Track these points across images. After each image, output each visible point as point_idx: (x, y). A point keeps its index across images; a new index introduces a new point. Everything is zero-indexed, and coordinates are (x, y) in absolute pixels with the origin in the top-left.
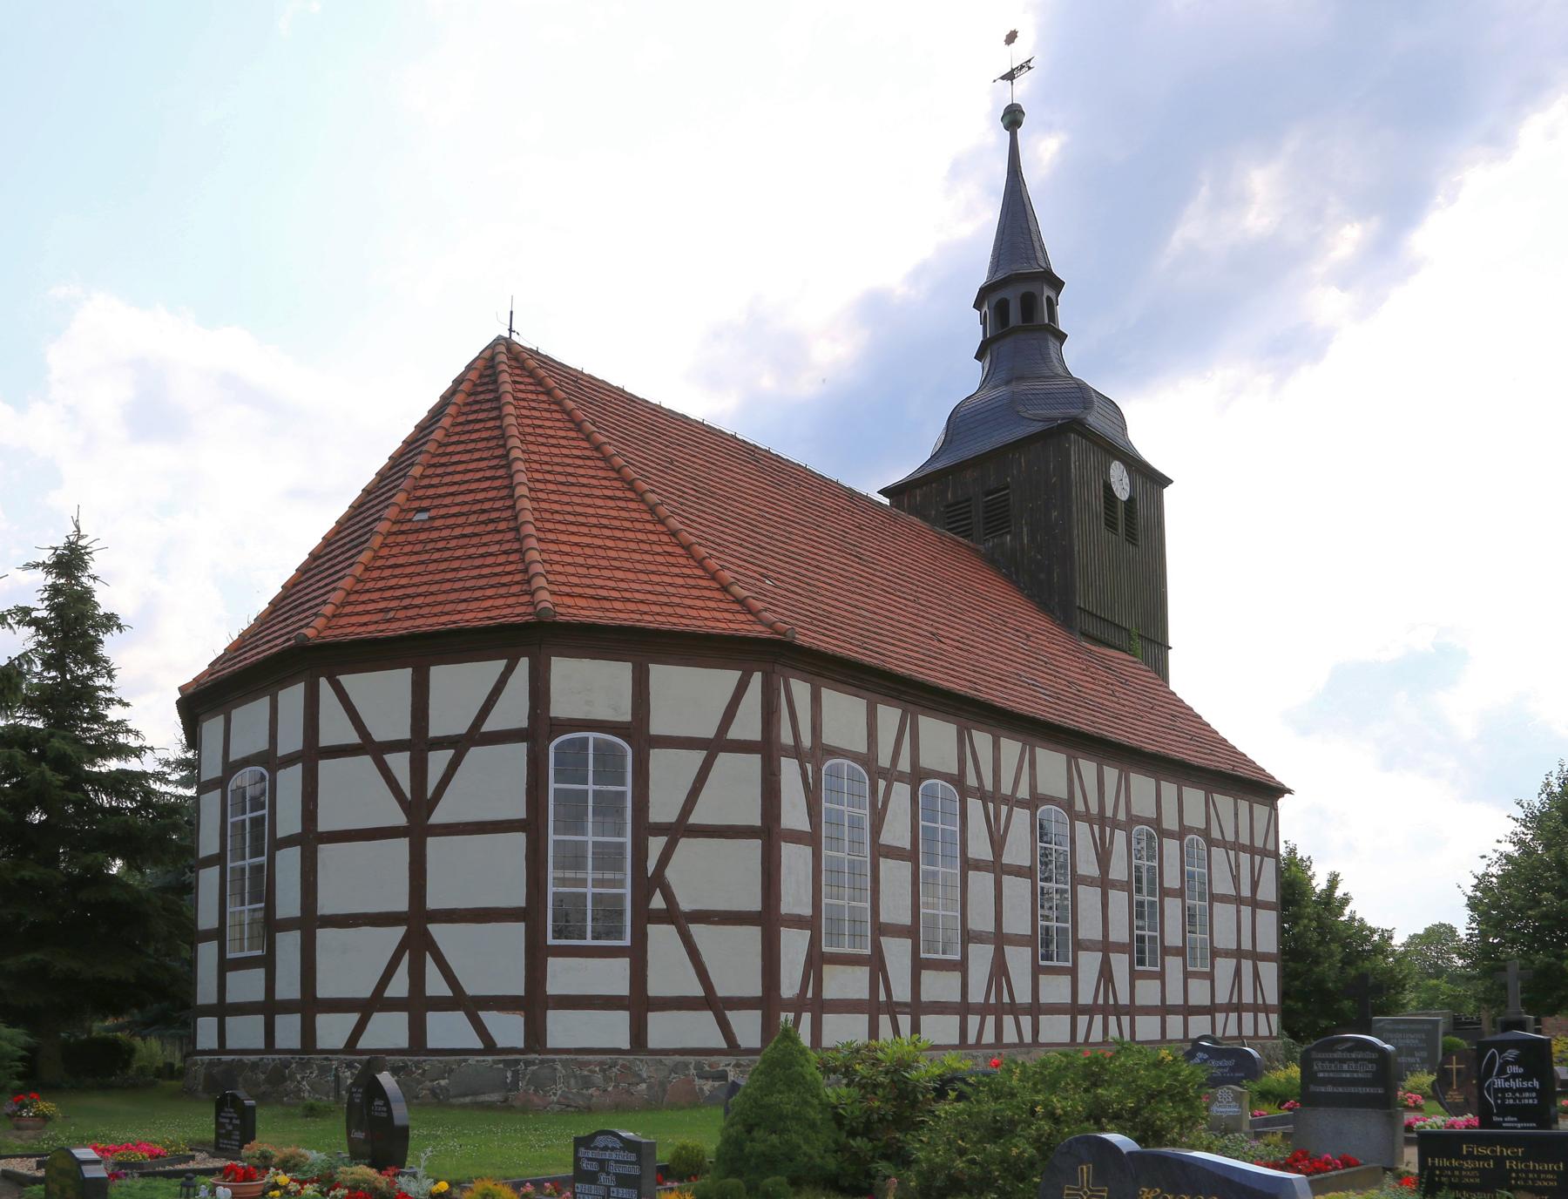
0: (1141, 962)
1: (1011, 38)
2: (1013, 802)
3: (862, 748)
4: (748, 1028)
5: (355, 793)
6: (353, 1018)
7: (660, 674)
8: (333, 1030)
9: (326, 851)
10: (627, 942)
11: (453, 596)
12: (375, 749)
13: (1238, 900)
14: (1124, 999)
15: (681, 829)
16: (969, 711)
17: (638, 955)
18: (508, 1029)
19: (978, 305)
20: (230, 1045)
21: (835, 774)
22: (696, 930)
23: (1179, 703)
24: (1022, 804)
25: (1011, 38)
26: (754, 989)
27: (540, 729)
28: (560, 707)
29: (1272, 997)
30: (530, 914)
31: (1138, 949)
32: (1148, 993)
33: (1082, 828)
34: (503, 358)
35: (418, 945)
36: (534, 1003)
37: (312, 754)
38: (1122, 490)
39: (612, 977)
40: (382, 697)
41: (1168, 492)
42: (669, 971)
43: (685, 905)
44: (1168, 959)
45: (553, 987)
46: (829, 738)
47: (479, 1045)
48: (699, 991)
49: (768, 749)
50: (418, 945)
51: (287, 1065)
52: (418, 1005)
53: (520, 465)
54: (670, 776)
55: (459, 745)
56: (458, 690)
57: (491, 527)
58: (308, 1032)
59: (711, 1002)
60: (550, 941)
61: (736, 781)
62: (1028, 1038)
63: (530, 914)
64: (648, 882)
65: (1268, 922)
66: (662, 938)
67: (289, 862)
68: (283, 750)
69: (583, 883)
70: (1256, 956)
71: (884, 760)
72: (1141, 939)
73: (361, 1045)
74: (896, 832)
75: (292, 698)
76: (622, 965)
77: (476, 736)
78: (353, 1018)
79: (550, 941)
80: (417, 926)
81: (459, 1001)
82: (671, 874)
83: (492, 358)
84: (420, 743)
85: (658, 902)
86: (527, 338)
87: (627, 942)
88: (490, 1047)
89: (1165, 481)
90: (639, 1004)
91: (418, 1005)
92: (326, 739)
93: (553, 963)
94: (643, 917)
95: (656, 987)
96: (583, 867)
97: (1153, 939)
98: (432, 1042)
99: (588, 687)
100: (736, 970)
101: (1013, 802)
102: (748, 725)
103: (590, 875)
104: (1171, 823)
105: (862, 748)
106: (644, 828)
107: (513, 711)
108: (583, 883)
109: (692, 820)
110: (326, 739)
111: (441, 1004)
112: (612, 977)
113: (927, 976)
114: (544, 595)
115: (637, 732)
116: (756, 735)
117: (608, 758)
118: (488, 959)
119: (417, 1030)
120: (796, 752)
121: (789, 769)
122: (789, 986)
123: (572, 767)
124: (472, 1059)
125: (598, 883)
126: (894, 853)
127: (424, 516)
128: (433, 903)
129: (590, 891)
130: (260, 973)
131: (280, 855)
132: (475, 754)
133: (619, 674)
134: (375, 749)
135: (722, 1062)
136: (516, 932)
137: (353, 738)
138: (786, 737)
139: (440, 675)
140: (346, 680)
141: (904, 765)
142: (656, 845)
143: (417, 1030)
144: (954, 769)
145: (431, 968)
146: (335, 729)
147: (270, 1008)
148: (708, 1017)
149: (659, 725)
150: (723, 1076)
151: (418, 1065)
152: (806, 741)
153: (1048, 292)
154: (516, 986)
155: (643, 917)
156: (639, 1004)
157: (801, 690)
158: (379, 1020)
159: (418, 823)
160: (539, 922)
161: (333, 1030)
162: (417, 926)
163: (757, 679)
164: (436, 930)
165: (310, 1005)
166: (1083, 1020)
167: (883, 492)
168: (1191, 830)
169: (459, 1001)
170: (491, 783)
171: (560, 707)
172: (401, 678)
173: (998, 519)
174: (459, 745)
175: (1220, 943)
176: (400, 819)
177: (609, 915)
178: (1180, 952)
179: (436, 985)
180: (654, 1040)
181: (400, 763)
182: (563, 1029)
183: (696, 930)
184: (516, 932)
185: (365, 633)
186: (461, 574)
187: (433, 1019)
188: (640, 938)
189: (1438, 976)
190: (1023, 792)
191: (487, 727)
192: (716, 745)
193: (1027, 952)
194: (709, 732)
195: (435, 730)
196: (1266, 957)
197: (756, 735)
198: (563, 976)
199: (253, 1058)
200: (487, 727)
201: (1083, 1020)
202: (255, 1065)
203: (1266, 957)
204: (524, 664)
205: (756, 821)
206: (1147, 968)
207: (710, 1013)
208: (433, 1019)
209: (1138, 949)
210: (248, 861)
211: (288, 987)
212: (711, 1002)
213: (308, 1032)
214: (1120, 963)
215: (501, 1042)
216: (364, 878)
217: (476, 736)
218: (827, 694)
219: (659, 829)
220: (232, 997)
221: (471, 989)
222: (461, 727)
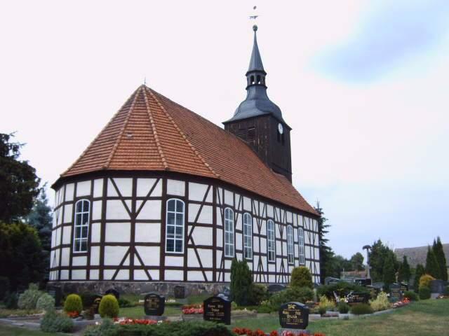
0: (270, 259)
1: (255, 8)
2: (263, 219)
3: (250, 210)
4: (209, 275)
5: (116, 210)
6: (114, 271)
7: (191, 184)
8: (108, 274)
9: (108, 225)
10: (183, 253)
11: (143, 160)
12: (121, 198)
13: (310, 245)
14: (265, 270)
15: (195, 224)
16: (254, 196)
17: (185, 256)
18: (155, 275)
19: (247, 75)
20: (73, 278)
21: (227, 210)
22: (198, 250)
23: (293, 188)
24: (264, 219)
25: (255, 8)
26: (211, 266)
27: (165, 197)
28: (169, 192)
29: (319, 273)
30: (161, 245)
31: (269, 255)
32: (272, 268)
33: (255, 219)
34: (144, 91)
35: (132, 252)
36: (162, 268)
37: (105, 198)
38: (281, 131)
39: (179, 261)
40: (125, 186)
41: (291, 131)
42: (192, 262)
43: (196, 244)
44: (255, 256)
45: (167, 264)
46: (226, 202)
47: (204, 280)
48: (199, 266)
49: (214, 205)
50: (132, 252)
51: (95, 284)
52: (132, 268)
53: (153, 125)
54: (193, 209)
55: (145, 199)
56: (144, 186)
57: (148, 141)
58: (101, 275)
59: (202, 269)
60: (166, 252)
61: (207, 211)
62: (266, 281)
63: (161, 245)
64: (188, 238)
65: (317, 251)
66: (191, 251)
67: (96, 228)
68: (95, 196)
69: (173, 237)
70: (315, 261)
71: (237, 208)
72: (270, 252)
73: (116, 278)
74: (239, 227)
75: (99, 183)
76: (85, 258)
77: (148, 198)
78: (114, 271)
79: (166, 252)
80: (132, 246)
81: (143, 267)
82: (193, 235)
83: (142, 91)
84: (134, 198)
85: (190, 243)
86: (149, 86)
87: (183, 253)
88: (150, 280)
89: (290, 129)
90: (186, 269)
91: (132, 268)
92: (109, 195)
93: (166, 258)
94: (187, 246)
95: (189, 265)
96: (173, 233)
97: (273, 253)
98: (135, 278)
99: (176, 188)
100: (207, 261)
101: (263, 219)
102: (210, 199)
103: (175, 235)
104: (295, 225)
105: (232, 205)
106: (187, 224)
107: (158, 192)
108: (173, 237)
109: (198, 222)
110: (109, 195)
111: (138, 268)
112: (179, 261)
113: (75, 259)
114: (165, 164)
115: (186, 199)
116: (211, 201)
117: (180, 205)
118: (151, 256)
119: (132, 275)
120: (219, 206)
121: (218, 209)
122: (218, 266)
123: (171, 208)
124: (147, 283)
125: (177, 237)
126: (239, 231)
127: (130, 135)
128: (136, 241)
129: (175, 239)
130: (85, 258)
131: (93, 225)
132: (148, 202)
133: (182, 184)
134: (121, 198)
135: (204, 284)
136: (158, 248)
137: (117, 195)
138: (218, 202)
139: (140, 181)
140: (115, 180)
141: (241, 209)
142: (190, 227)
143: (132, 275)
144: (250, 210)
145: (136, 259)
146: (112, 192)
147: (88, 268)
148: (201, 273)
149: (190, 198)
150: (204, 288)
151: (132, 284)
152: (222, 203)
153: (262, 75)
154: (157, 263)
155: (187, 246)
156: (186, 269)
157: (220, 190)
158: (121, 271)
159: (133, 219)
160: (166, 247)
161: (108, 274)
162: (132, 246)
163: (212, 187)
164: (137, 248)
165: (102, 267)
166: (278, 276)
167: (223, 123)
168: (300, 226)
169: (143, 267)
170: (152, 210)
171: (169, 192)
172: (129, 181)
173: (252, 135)
174: (145, 199)
175: (307, 257)
176: (129, 218)
177: (84, 244)
178: (298, 259)
179: (137, 263)
180: (189, 278)
181: (129, 203)
182: (169, 275)
183: (198, 250)
184: (158, 248)
185: (227, 181)
186: (143, 154)
187: (136, 272)
188: (186, 251)
189: (247, 277)
190: (264, 217)
191: (151, 195)
192: (203, 203)
193: (266, 258)
194: (201, 200)
195: (139, 195)
196: (317, 261)
197: (211, 201)
198: (169, 261)
199: (65, 282)
200: (151, 195)
201: (278, 276)
202: (83, 284)
203: (317, 261)
204: (161, 180)
205: (211, 223)
206: (271, 261)
207: (143, 271)
208: (136, 272)
209: (269, 255)
210: (82, 226)
211: (95, 261)
212: (202, 269)
213: (101, 275)
214: (264, 259)
215: (153, 278)
216: (118, 233)
217: (148, 198)
218: (226, 192)
219: (191, 224)
220: (74, 264)
221: (146, 264)
222: (145, 195)
